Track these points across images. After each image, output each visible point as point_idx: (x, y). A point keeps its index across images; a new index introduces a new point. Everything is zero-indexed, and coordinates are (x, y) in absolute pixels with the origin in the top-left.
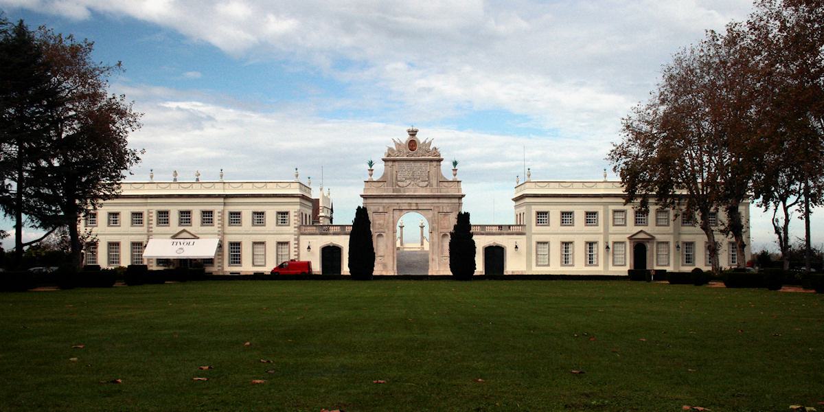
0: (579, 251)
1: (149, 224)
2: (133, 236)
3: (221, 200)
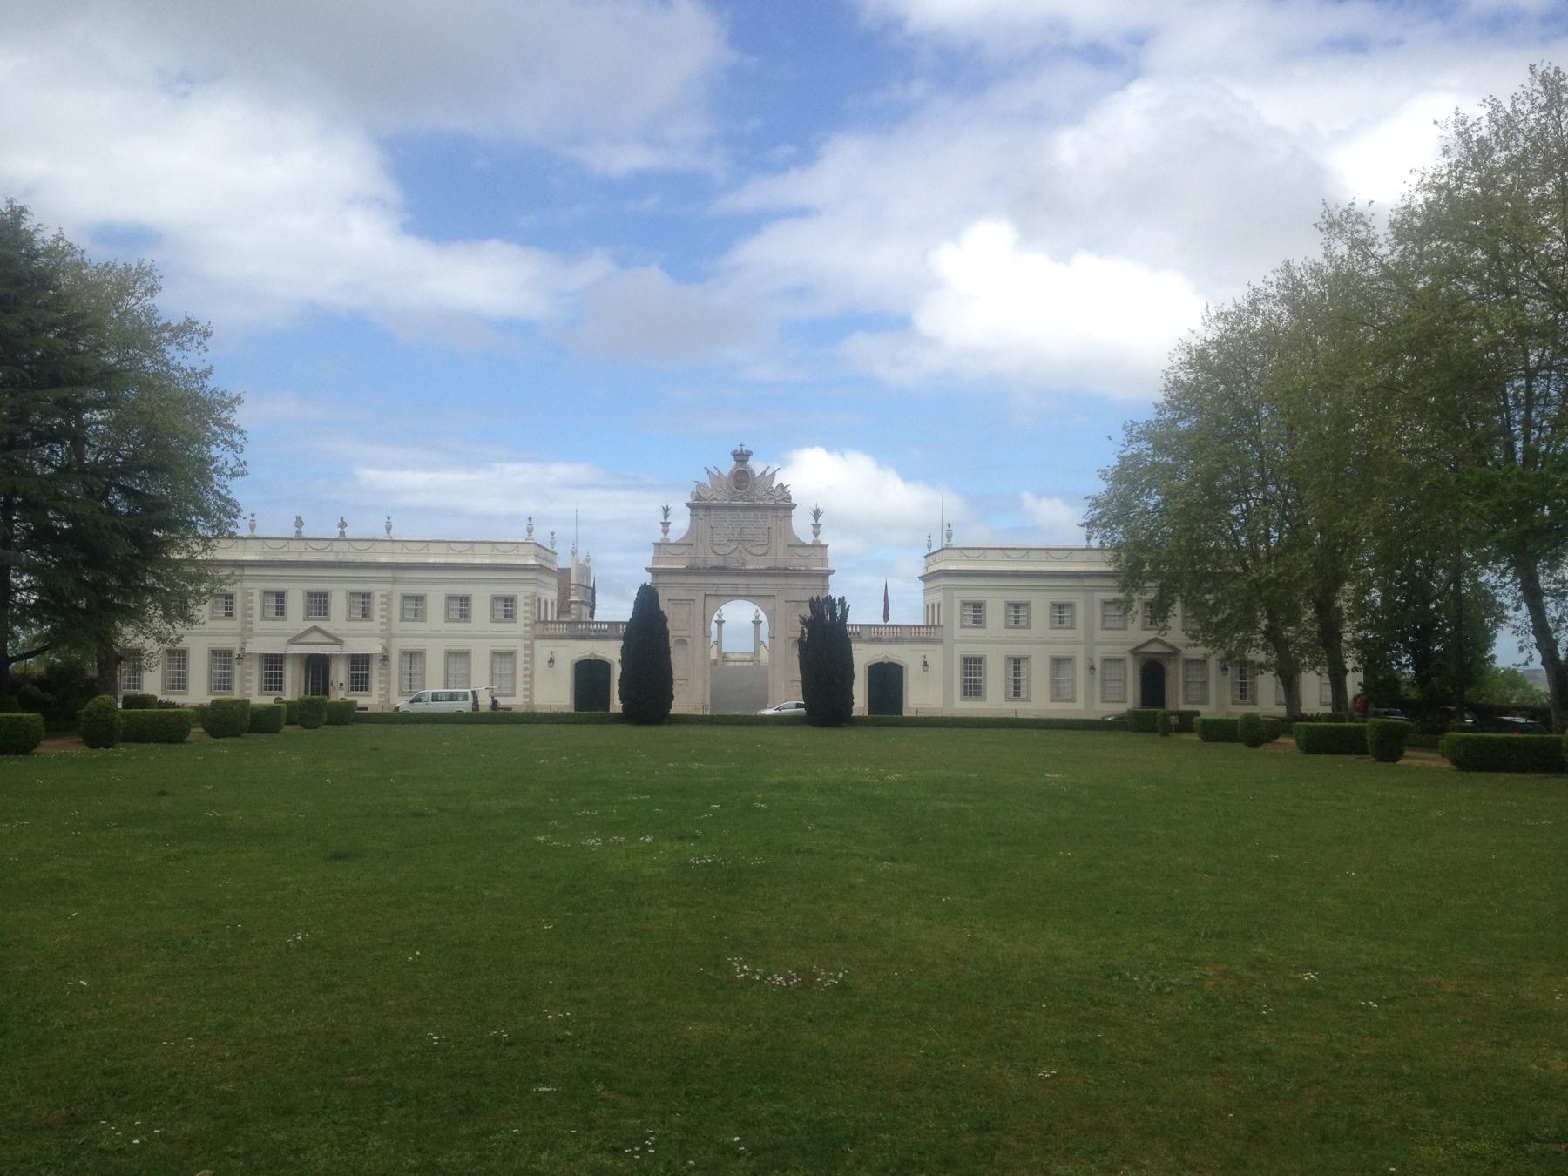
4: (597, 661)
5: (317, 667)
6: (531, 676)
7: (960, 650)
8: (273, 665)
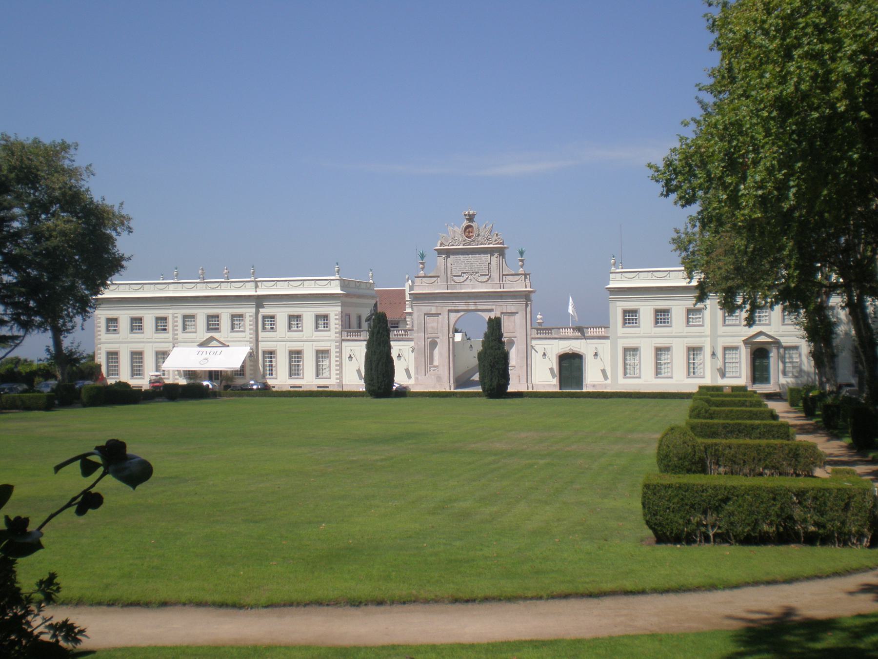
6: (341, 366)
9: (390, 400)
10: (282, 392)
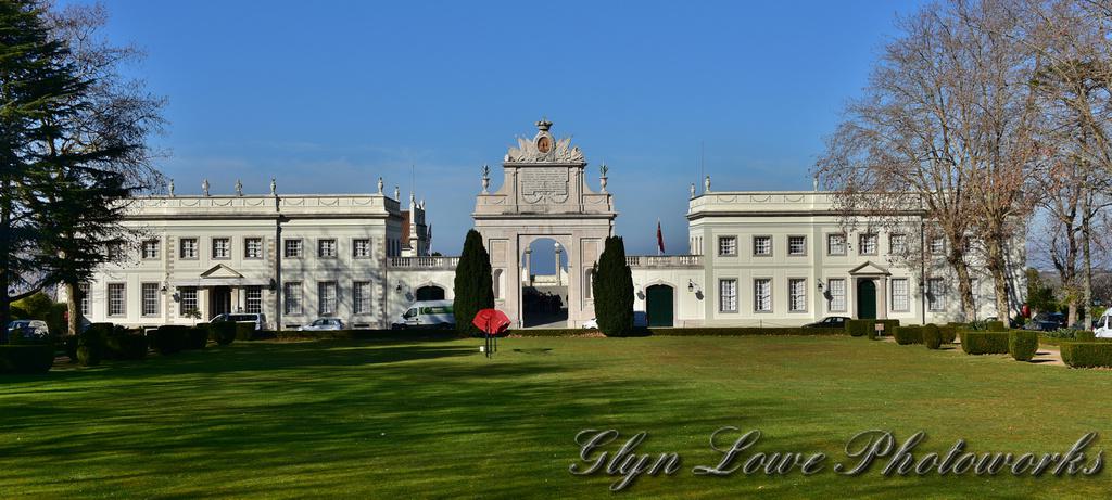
0: (133, 299)
1: (168, 257)
2: (145, 274)
3: (839, 219)
4: (663, 286)
5: (220, 296)
7: (718, 274)
8: (186, 295)
9: (628, 340)
10: (794, 328)
